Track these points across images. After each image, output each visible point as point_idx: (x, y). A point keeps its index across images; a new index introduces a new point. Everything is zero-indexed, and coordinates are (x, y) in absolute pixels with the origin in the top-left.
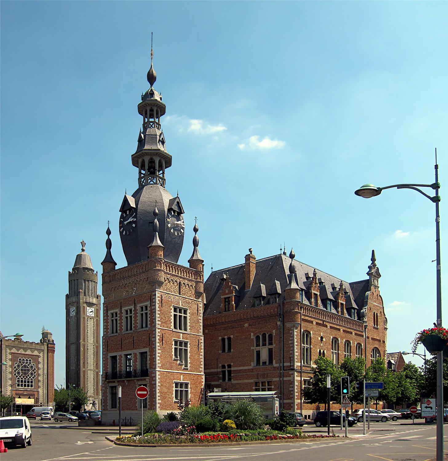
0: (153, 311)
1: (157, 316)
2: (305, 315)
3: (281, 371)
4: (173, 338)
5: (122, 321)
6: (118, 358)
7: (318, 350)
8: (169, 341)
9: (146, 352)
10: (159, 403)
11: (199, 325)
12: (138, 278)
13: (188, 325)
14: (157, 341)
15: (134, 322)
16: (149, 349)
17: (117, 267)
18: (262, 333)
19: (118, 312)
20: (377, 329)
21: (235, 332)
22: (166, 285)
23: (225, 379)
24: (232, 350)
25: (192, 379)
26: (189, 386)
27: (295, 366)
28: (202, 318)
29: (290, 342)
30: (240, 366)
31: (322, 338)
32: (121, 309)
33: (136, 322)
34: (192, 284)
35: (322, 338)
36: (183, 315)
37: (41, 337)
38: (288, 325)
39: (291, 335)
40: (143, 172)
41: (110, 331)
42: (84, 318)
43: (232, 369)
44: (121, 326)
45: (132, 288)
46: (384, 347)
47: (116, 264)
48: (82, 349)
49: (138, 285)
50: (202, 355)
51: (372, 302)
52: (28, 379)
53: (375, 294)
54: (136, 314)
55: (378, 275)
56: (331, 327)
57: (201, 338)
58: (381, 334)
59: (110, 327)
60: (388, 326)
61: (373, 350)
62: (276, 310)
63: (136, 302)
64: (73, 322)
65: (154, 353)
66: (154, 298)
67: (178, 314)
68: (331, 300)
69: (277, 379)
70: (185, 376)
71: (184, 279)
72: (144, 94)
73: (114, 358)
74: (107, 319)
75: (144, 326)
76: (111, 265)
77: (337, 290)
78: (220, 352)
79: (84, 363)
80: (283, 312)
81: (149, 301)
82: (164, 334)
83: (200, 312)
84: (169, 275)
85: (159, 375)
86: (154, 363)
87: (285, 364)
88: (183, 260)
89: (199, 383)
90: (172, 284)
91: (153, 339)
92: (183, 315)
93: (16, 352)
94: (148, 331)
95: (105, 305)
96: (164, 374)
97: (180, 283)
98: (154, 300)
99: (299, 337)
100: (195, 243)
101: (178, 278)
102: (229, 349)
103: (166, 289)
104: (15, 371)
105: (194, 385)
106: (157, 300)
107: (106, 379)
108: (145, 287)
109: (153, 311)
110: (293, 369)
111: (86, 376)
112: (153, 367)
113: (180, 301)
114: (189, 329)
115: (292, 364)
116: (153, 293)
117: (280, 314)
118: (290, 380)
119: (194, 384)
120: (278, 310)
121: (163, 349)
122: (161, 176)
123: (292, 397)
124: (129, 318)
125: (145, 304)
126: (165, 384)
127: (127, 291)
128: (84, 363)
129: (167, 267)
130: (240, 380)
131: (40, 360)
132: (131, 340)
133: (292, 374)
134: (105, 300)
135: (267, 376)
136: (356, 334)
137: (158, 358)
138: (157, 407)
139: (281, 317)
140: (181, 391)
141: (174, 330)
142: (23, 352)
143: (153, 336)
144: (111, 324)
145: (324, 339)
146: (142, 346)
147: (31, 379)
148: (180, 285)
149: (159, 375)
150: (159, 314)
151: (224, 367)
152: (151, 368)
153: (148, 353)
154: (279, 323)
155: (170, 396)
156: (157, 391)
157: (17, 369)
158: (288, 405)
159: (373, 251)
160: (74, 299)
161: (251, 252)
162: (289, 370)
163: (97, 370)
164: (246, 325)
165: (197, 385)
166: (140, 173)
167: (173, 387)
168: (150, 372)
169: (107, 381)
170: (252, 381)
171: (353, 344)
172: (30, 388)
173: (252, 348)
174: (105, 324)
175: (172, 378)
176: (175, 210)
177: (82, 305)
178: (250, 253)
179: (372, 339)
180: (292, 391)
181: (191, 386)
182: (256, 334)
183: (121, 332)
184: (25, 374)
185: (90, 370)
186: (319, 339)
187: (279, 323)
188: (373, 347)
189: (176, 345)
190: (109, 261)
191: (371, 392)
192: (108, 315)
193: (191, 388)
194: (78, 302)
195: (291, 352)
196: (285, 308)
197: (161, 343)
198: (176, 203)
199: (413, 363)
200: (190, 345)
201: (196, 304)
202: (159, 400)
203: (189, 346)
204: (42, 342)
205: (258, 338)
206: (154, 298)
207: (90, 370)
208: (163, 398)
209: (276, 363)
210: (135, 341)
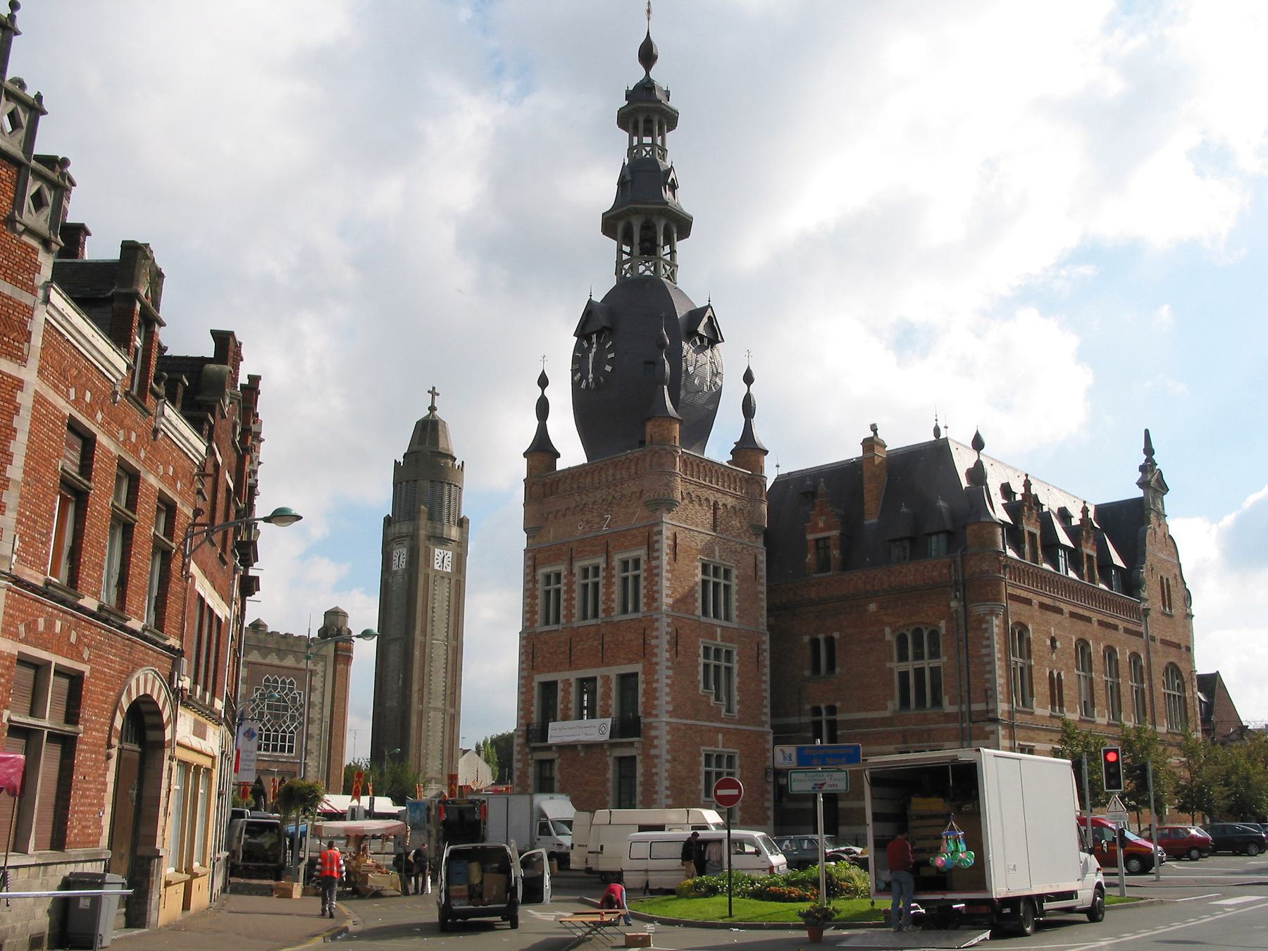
1: (666, 583)
2: (1013, 586)
6: (560, 686)
9: (636, 675)
17: (561, 465)
18: (912, 628)
19: (564, 573)
20: (1171, 616)
22: (685, 510)
24: (838, 670)
26: (737, 762)
27: (1000, 711)
28: (764, 589)
29: (984, 651)
30: (859, 711)
31: (1053, 640)
33: (609, 599)
35: (1053, 640)
36: (722, 581)
37: (319, 623)
40: (627, 249)
41: (539, 617)
42: (427, 576)
43: (839, 717)
44: (570, 607)
45: (601, 516)
46: (1190, 661)
47: (558, 455)
48: (417, 653)
51: (1153, 552)
52: (284, 731)
54: (609, 577)
55: (1162, 488)
56: (1073, 615)
59: (540, 608)
60: (1195, 609)
61: (1167, 669)
62: (945, 571)
64: (398, 583)
66: (657, 541)
67: (712, 579)
68: (1065, 548)
71: (724, 493)
72: (631, 88)
73: (549, 689)
74: (535, 588)
75: (630, 607)
77: (1019, 497)
78: (807, 673)
79: (421, 690)
88: (719, 448)
92: (722, 581)
93: (260, 660)
94: (640, 620)
97: (716, 503)
100: (748, 408)
102: (831, 666)
104: (253, 710)
106: (665, 546)
107: (528, 740)
108: (634, 513)
110: (995, 720)
111: (424, 726)
113: (717, 549)
115: (991, 707)
117: (956, 582)
122: (668, 257)
127: (588, 522)
128: (421, 690)
131: (317, 681)
132: (596, 643)
133: (993, 732)
141: (703, 619)
142: (276, 662)
143: (655, 633)
145: (1058, 644)
147: (292, 732)
148: (715, 510)
150: (668, 580)
151: (817, 711)
152: (648, 714)
153: (641, 678)
154: (953, 604)
157: (258, 706)
159: (1147, 432)
160: (404, 528)
163: (452, 710)
164: (873, 607)
166: (620, 251)
171: (1123, 656)
172: (286, 754)
177: (422, 543)
178: (872, 434)
179: (1164, 642)
183: (569, 621)
184: (277, 717)
185: (435, 709)
186: (1048, 642)
187: (953, 604)
188: (1165, 662)
190: (542, 450)
193: (741, 766)
194: (413, 537)
198: (705, 320)
204: (324, 633)
205: (902, 640)
207: (435, 709)
209: (951, 704)
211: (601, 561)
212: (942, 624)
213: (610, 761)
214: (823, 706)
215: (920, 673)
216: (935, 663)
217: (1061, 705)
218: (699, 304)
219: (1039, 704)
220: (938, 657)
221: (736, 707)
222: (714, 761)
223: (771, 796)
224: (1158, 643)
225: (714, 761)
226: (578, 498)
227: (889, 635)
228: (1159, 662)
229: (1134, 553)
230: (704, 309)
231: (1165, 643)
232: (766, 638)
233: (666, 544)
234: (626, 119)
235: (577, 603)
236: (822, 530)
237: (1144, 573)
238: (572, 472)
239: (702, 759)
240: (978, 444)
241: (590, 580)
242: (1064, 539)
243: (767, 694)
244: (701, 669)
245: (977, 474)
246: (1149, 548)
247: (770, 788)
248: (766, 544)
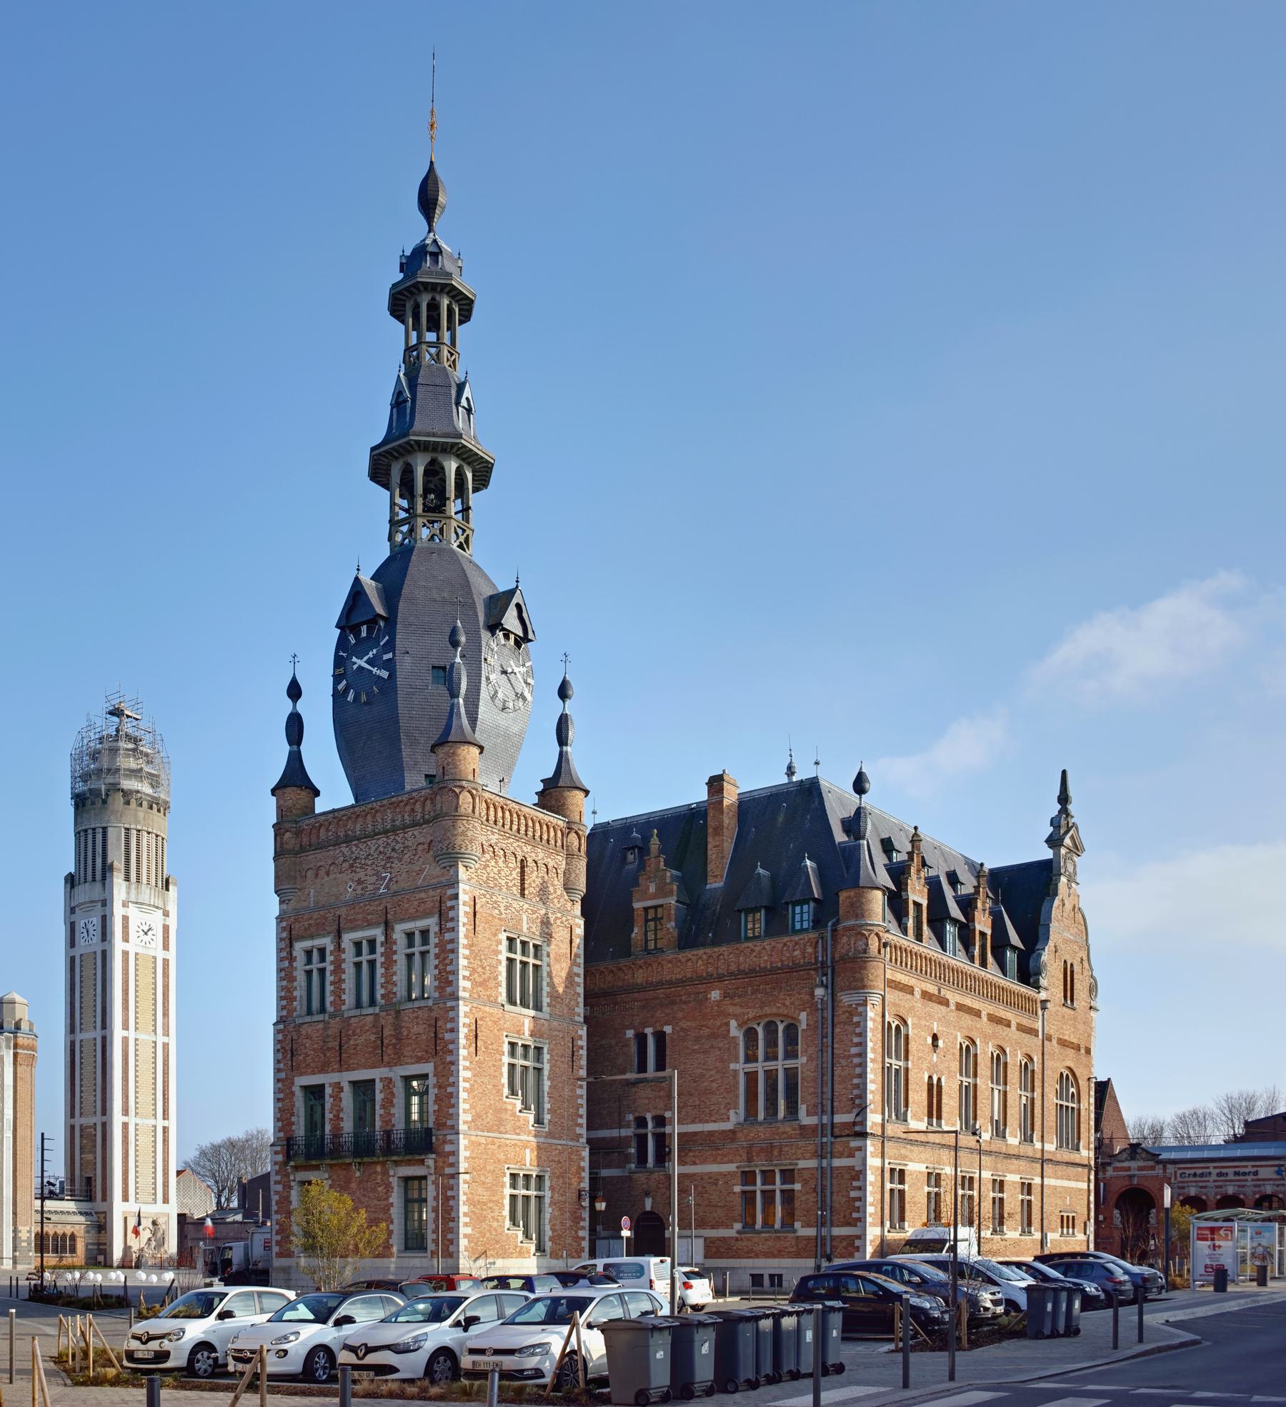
0: (449, 947)
1: (462, 962)
3: (825, 1140)
5: (343, 977)
6: (328, 1091)
10: (465, 1236)
12: (397, 842)
13: (544, 994)
14: (462, 1041)
15: (383, 980)
16: (436, 1068)
17: (321, 805)
23: (646, 1161)
27: (869, 1124)
30: (693, 1122)
31: (935, 1038)
32: (340, 937)
35: (935, 1038)
36: (531, 961)
38: (846, 999)
39: (858, 1030)
41: (299, 1006)
44: (338, 992)
49: (396, 864)
51: (1059, 930)
53: (1068, 906)
54: (389, 954)
56: (960, 1007)
58: (1081, 1027)
62: (810, 950)
63: (389, 917)
65: (451, 1080)
69: (812, 1163)
72: (408, 253)
76: (304, 794)
80: (833, 958)
81: (437, 916)
85: (466, 1148)
86: (451, 1111)
87: (838, 1118)
90: (501, 863)
91: (448, 1036)
92: (531, 961)
94: (431, 1009)
95: (284, 924)
98: (451, 914)
99: (880, 1036)
105: (561, 1181)
106: (461, 914)
107: (288, 1157)
108: (422, 870)
109: (449, 947)
112: (450, 1123)
113: (525, 918)
114: (549, 1005)
116: (450, 892)
119: (561, 1176)
120: (816, 952)
121: (478, 1070)
123: (859, 1219)
124: (365, 966)
125: (422, 924)
126: (483, 1178)
127: (359, 882)
129: (488, 808)
130: (695, 1163)
133: (859, 1149)
134: (285, 906)
135: (781, 1151)
137: (463, 1095)
138: (462, 1248)
139: (826, 975)
140: (527, 1198)
144: (304, 984)
145: (940, 1043)
146: (411, 1057)
148: (522, 868)
149: (466, 1148)
154: (819, 992)
156: (462, 1198)
158: (845, 1244)
159: (1064, 772)
160: (93, 891)
162: (848, 1135)
164: (715, 995)
167: (503, 1186)
168: (437, 1140)
169: (292, 1163)
170: (732, 1167)
174: (284, 983)
175: (502, 1157)
180: (859, 1199)
182: (745, 1023)
186: (930, 1040)
187: (819, 992)
189: (512, 1054)
190: (295, 779)
192: (295, 954)
193: (552, 1188)
196: (839, 947)
197: (473, 1049)
199: (1180, 1113)
202: (466, 1224)
203: (546, 1057)
205: (750, 1035)
206: (452, 908)
208: (478, 1219)
210: (386, 1041)
211: (378, 933)
212: (803, 1016)
213: (394, 1182)
214: (649, 1117)
215: (771, 1076)
216: (790, 1063)
217: (939, 1117)
218: (502, 587)
219: (914, 1116)
220: (796, 1057)
221: (547, 1117)
222: (521, 1182)
223: (586, 1224)
224: (1054, 1041)
225: (521, 1182)
226: (345, 850)
227: (735, 1031)
228: (1057, 1063)
229: (1034, 933)
230: (511, 593)
231: (1063, 1043)
232: (583, 1032)
233: (463, 911)
234: (401, 303)
235: (349, 985)
236: (654, 897)
237: (1046, 956)
238: (335, 815)
239: (507, 1179)
240: (860, 785)
241: (365, 957)
242: (955, 911)
243: (583, 1102)
244: (505, 1070)
245: (854, 825)
246: (1054, 926)
247: (586, 1215)
248: (583, 913)
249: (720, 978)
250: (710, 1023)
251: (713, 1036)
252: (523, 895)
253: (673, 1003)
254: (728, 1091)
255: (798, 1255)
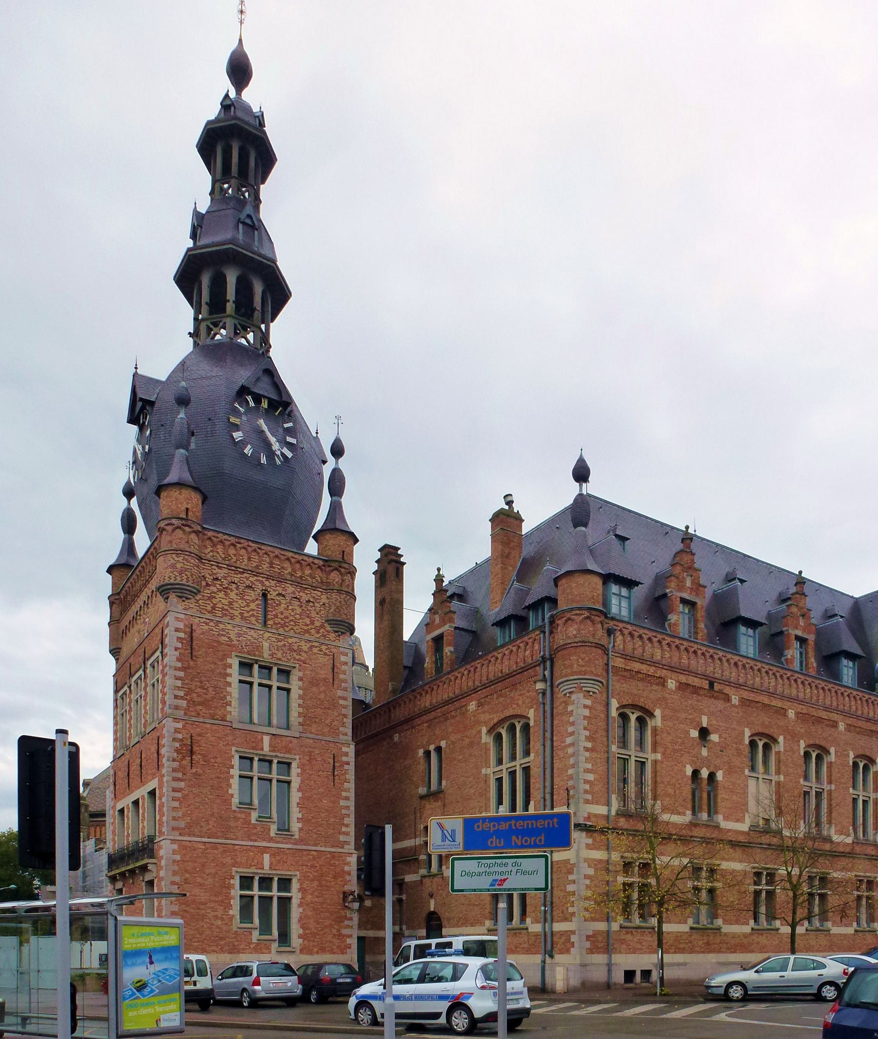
4: (234, 749)
7: (689, 771)
8: (216, 758)
11: (340, 714)
21: (450, 730)
25: (307, 866)
31: (704, 733)
34: (314, 597)
35: (704, 733)
50: (347, 798)
57: (344, 749)
70: (278, 858)
82: (200, 735)
83: (342, 676)
84: (220, 568)
89: (335, 877)
96: (195, 849)
101: (257, 580)
103: (209, 608)
105: (316, 883)
118: (567, 861)
126: (199, 880)
136: (849, 727)
145: (714, 737)
155: (219, 913)
161: (510, 503)
164: (472, 706)
165: (327, 881)
173: (484, 771)
176: (262, 393)
181: (305, 886)
186: (695, 734)
191: (506, 865)
195: (570, 772)
200: (303, 770)
201: (325, 654)
249: (475, 690)
250: (468, 733)
251: (471, 745)
252: (265, 623)
253: (447, 719)
254: (481, 795)
255: (528, 951)
